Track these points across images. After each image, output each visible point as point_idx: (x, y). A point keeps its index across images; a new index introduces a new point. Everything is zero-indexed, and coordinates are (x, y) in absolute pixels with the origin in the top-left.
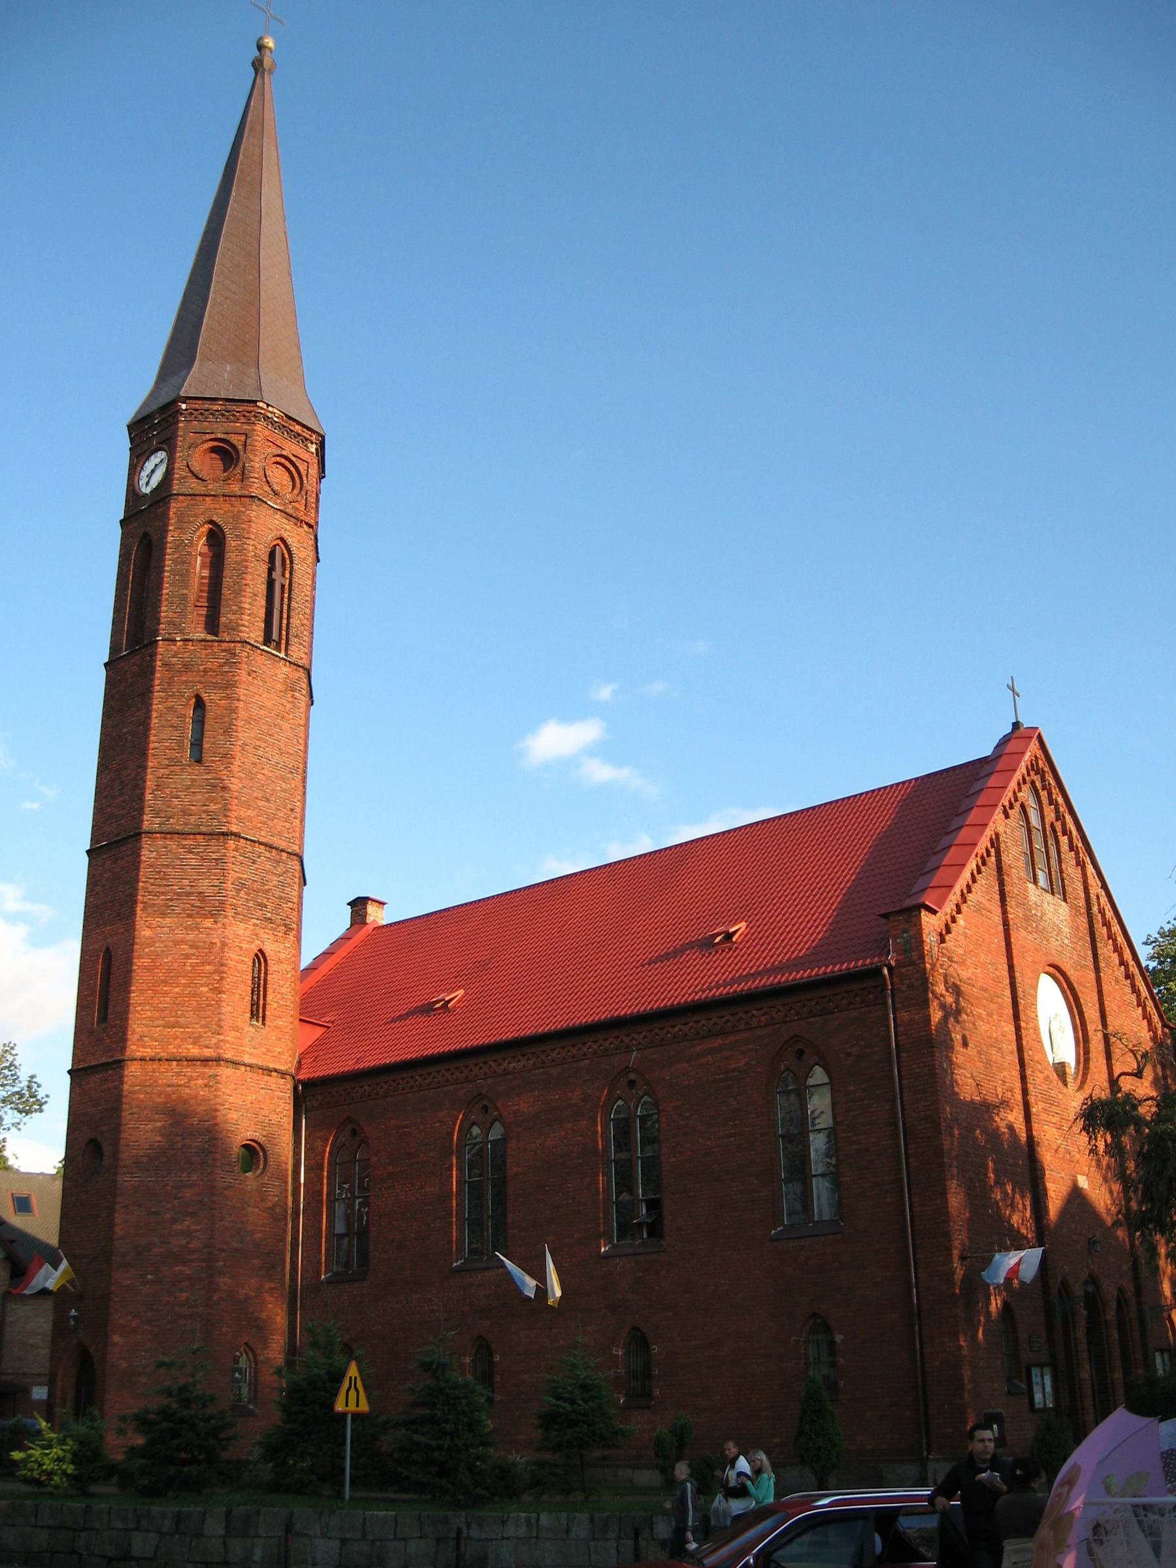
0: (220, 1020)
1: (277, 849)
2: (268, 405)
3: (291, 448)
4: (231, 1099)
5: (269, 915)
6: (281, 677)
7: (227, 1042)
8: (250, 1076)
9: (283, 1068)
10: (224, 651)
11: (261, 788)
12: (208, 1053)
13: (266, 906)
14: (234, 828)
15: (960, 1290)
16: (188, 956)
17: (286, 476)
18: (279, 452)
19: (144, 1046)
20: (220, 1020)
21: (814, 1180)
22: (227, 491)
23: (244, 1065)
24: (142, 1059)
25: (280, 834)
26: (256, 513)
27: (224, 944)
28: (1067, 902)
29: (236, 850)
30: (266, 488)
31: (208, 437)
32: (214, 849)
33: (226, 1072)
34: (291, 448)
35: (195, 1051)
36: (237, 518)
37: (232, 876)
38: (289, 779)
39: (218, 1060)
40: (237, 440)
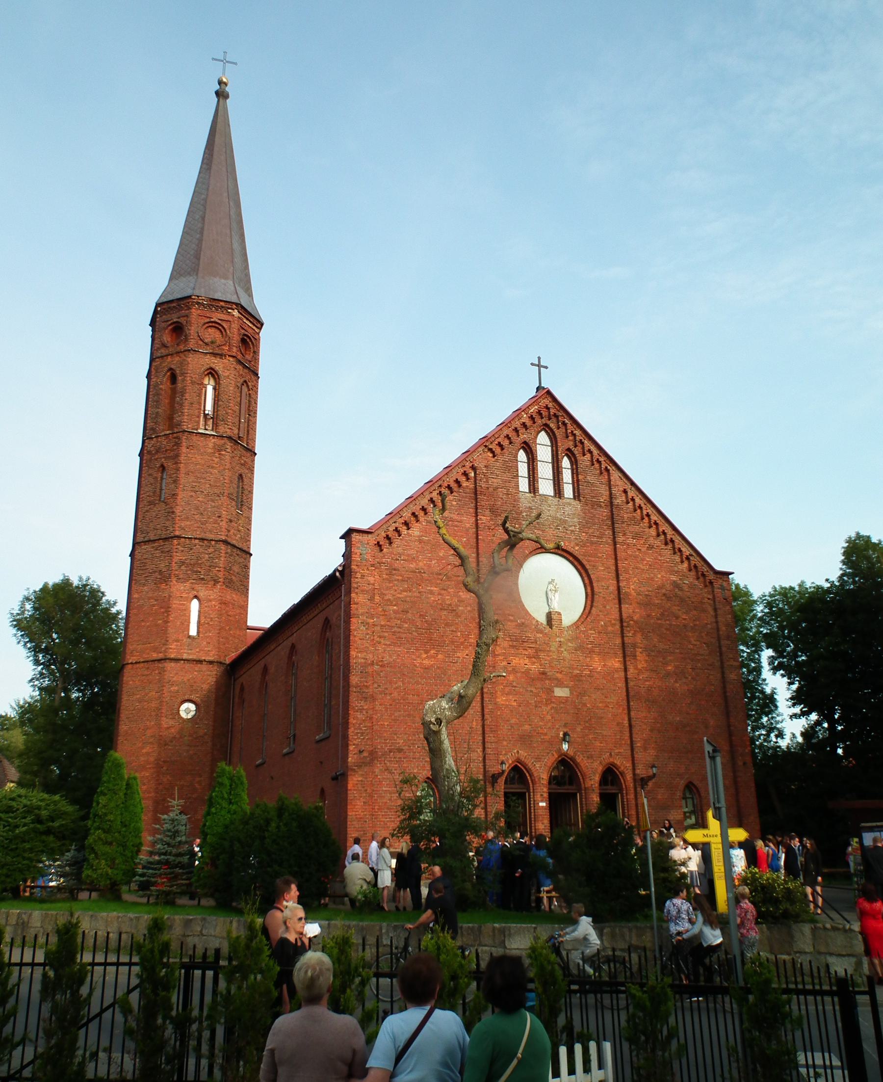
0: (167, 637)
1: (207, 540)
2: (198, 296)
3: (217, 316)
4: (174, 679)
5: (202, 576)
6: (211, 445)
7: (171, 648)
8: (188, 666)
9: (211, 659)
10: (174, 438)
11: (197, 508)
12: (161, 656)
13: (200, 572)
14: (177, 533)
15: (522, 1054)
16: (154, 605)
17: (218, 332)
18: (208, 320)
19: (133, 656)
20: (167, 637)
21: (196, 961)
22: (178, 349)
23: (182, 660)
24: (132, 663)
25: (210, 531)
26: (191, 359)
27: (170, 596)
28: (579, 500)
29: (179, 544)
30: (201, 343)
31: (170, 322)
32: (167, 546)
33: (170, 665)
34: (217, 316)
35: (155, 656)
36: (182, 364)
37: (176, 559)
38: (217, 500)
39: (165, 659)
40: (182, 320)
